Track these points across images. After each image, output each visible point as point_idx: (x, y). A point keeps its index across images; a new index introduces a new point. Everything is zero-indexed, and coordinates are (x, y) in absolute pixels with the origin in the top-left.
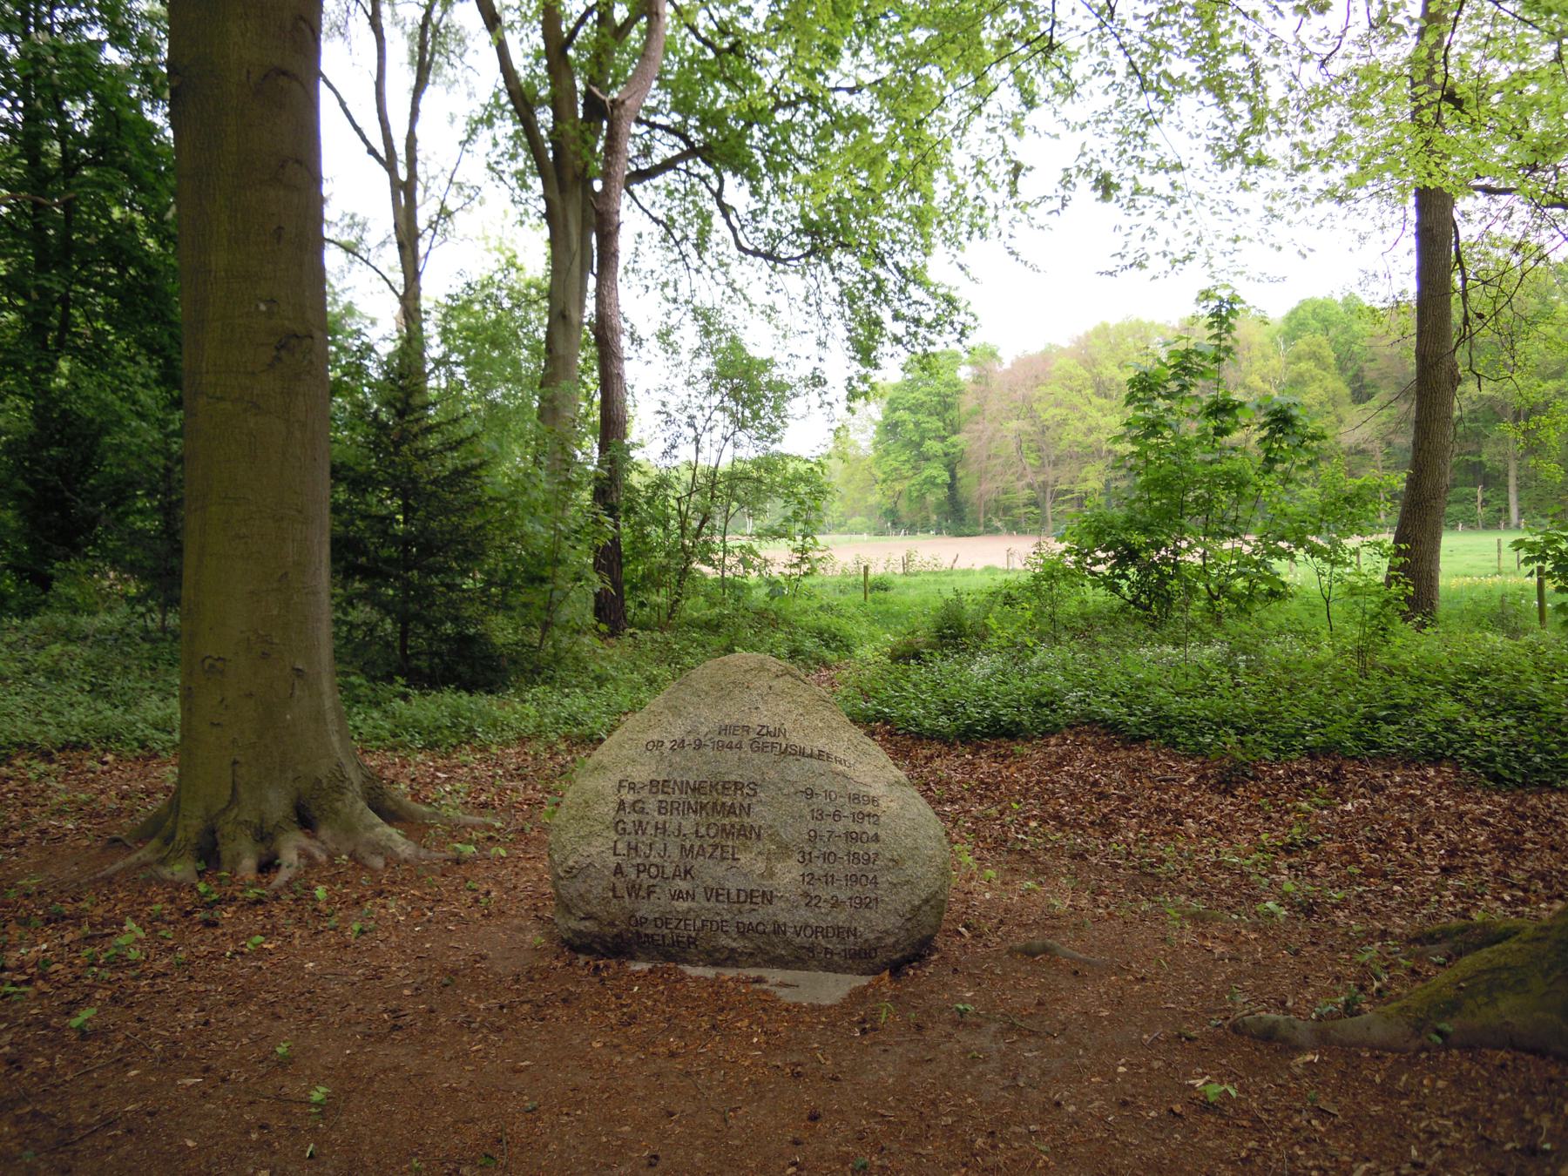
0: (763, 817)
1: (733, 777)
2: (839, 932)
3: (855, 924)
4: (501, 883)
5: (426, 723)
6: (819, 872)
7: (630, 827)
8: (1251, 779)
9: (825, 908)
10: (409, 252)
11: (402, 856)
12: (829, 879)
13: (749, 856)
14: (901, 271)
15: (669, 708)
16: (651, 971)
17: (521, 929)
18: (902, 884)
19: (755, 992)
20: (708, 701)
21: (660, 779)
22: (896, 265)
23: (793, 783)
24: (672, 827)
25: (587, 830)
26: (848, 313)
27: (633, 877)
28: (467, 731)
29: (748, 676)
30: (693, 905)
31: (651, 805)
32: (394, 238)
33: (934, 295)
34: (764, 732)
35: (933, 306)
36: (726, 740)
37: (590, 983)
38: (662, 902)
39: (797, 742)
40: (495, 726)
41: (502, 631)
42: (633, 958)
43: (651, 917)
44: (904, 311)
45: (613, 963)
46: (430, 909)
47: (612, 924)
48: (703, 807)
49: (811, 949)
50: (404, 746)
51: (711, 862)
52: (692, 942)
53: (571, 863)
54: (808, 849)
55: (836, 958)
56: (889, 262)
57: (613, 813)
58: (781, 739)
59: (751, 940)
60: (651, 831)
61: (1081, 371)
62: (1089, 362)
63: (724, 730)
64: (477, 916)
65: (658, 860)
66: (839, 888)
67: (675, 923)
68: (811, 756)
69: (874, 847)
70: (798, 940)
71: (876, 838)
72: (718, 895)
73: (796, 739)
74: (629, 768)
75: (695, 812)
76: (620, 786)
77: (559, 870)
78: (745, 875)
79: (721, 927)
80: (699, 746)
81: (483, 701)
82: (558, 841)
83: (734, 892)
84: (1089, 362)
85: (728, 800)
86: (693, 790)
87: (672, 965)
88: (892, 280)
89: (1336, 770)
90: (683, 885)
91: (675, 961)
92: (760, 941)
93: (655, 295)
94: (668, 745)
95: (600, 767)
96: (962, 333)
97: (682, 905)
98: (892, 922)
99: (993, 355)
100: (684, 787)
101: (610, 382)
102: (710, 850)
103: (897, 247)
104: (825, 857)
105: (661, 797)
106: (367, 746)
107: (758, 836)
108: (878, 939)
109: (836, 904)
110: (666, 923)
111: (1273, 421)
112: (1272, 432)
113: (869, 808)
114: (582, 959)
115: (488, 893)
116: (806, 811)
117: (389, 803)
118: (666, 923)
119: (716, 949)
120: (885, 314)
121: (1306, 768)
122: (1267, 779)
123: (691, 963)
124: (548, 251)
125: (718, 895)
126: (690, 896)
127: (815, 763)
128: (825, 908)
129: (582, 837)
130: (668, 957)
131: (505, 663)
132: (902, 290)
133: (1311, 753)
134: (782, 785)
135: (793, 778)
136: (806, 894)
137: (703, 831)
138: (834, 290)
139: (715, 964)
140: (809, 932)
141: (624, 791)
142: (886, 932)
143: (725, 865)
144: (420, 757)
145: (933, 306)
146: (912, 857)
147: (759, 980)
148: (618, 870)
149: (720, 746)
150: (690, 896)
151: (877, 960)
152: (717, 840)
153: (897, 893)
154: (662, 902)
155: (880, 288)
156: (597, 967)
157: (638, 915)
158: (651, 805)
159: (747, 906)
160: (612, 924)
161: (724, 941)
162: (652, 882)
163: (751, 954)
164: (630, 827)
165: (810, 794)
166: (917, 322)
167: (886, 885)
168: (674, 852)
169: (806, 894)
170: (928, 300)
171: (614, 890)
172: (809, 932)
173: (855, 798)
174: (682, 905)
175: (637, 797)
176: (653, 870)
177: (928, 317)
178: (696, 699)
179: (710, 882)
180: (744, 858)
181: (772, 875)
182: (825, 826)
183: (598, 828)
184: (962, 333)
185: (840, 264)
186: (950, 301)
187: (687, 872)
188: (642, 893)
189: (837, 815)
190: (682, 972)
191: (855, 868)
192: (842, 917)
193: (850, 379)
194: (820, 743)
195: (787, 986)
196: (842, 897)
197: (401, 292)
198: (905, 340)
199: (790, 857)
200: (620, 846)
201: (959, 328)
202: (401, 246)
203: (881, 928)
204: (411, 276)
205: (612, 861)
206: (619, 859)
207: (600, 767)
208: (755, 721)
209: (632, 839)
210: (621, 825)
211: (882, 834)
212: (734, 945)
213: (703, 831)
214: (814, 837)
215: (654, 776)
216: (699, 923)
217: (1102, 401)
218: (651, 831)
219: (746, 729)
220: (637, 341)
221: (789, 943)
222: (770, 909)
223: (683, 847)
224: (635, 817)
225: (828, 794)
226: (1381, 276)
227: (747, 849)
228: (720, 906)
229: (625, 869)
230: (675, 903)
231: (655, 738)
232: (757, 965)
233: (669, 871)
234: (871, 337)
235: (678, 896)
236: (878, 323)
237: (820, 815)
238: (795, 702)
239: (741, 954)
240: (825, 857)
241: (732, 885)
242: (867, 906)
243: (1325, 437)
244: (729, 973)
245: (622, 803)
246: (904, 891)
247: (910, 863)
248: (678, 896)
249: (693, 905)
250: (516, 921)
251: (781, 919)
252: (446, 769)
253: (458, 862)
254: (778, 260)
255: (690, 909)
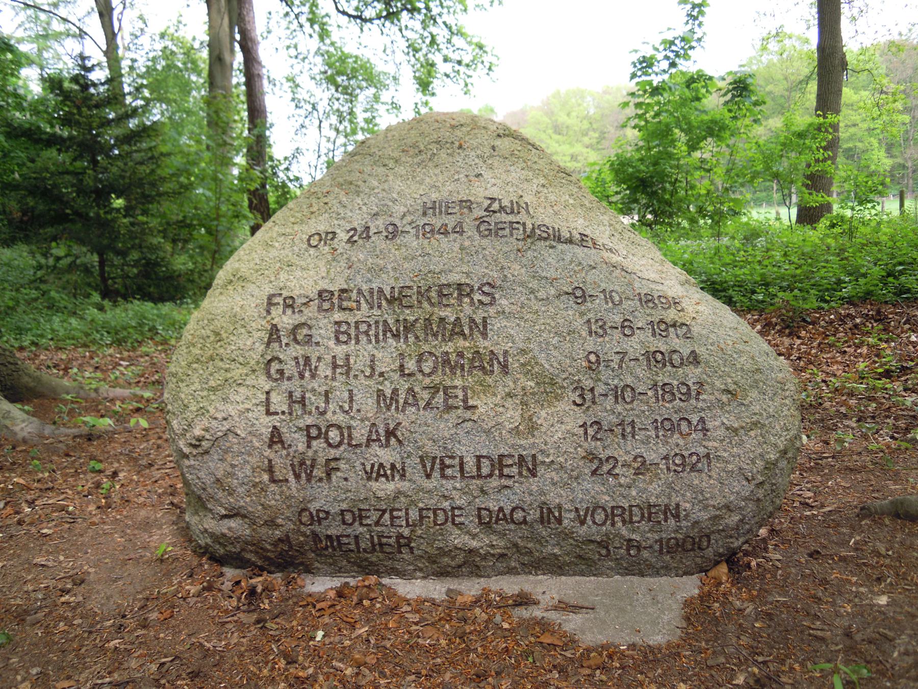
0: (510, 337)
1: (454, 278)
2: (649, 511)
3: (675, 499)
4: (136, 460)
5: (113, 324)
6: (609, 420)
7: (290, 368)
8: (809, 323)
9: (625, 476)
10: (106, 19)
11: (21, 435)
12: (626, 429)
13: (491, 401)
14: (449, 28)
15: (340, 185)
16: (340, 594)
17: (147, 525)
18: (748, 429)
19: (522, 622)
20: (401, 170)
21: (335, 288)
22: (444, 23)
23: (552, 281)
24: (359, 363)
25: (220, 376)
26: (413, 60)
27: (301, 447)
28: (150, 330)
29: (458, 133)
30: (405, 485)
31: (323, 329)
32: (96, 9)
33: (470, 43)
34: (493, 207)
35: (470, 51)
36: (437, 222)
37: (240, 625)
38: (352, 484)
39: (547, 221)
40: (173, 325)
41: (181, 263)
42: (309, 570)
43: (334, 509)
44: (451, 55)
45: (277, 578)
46: (31, 503)
47: (271, 523)
48: (409, 327)
49: (603, 545)
50: (94, 342)
51: (429, 415)
52: (404, 543)
53: (198, 432)
54: (588, 383)
55: (645, 554)
56: (438, 20)
57: (261, 348)
58: (522, 217)
59: (502, 535)
60: (324, 370)
61: (546, 119)
62: (550, 113)
63: (431, 208)
64: (92, 508)
65: (340, 418)
66: (646, 442)
67: (375, 516)
68: (570, 241)
69: (693, 374)
70: (583, 530)
71: (695, 359)
72: (443, 467)
73: (544, 217)
74: (283, 276)
75: (396, 336)
76: (270, 303)
77: (181, 444)
78: (488, 432)
79: (452, 517)
80: (393, 233)
81: (166, 308)
82: (176, 398)
83: (470, 462)
84: (550, 113)
85: (449, 314)
86: (390, 302)
87: (373, 579)
88: (441, 33)
89: (879, 312)
90: (386, 455)
91: (378, 573)
92: (516, 535)
93: (283, 52)
94: (343, 236)
95: (239, 279)
96: (490, 69)
97: (385, 488)
98: (739, 488)
99: (492, 111)
100: (376, 297)
101: (256, 112)
102: (426, 395)
103: (445, 11)
104: (618, 394)
105: (338, 316)
106: (61, 344)
107: (505, 367)
108: (715, 518)
109: (642, 467)
110: (360, 517)
111: (734, 89)
112: (734, 96)
113: (671, 315)
114: (230, 573)
115: (115, 474)
116: (579, 323)
117: (26, 379)
118: (360, 517)
119: (442, 552)
120: (437, 58)
121: (852, 311)
122: (822, 323)
123: (401, 574)
124: (206, 19)
125: (443, 467)
126: (398, 471)
127: (579, 251)
128: (625, 476)
129: (214, 389)
130: (366, 568)
131: (182, 281)
132: (449, 41)
133: (850, 302)
134: (534, 284)
135: (551, 274)
136: (591, 456)
137: (411, 365)
138: (403, 44)
139: (442, 573)
140: (600, 517)
141: (276, 312)
142: (727, 507)
143: (452, 417)
144: (111, 351)
145: (470, 51)
146: (755, 385)
147: (524, 600)
148: (276, 438)
149: (426, 232)
150: (398, 471)
151: (709, 552)
152: (437, 379)
153: (741, 444)
154: (352, 484)
155: (433, 42)
156: (252, 592)
157: (313, 507)
158: (323, 329)
159: (495, 482)
160: (271, 523)
161: (458, 539)
162: (333, 453)
163: (503, 556)
164: (290, 368)
165: (580, 296)
166: (459, 63)
167: (721, 432)
168: (367, 404)
169: (591, 456)
170: (466, 46)
171: (270, 470)
172: (600, 517)
173: (648, 300)
174: (385, 488)
175: (298, 319)
176: (334, 434)
177: (467, 59)
178: (381, 170)
179: (431, 449)
180: (483, 405)
181: (532, 428)
182: (612, 344)
183: (237, 372)
184: (490, 69)
185: (406, 26)
186: (481, 47)
187: (390, 433)
188: (318, 472)
189: (627, 327)
190: (392, 593)
191: (667, 409)
192: (655, 488)
193: (416, 104)
194: (577, 224)
195: (575, 608)
196: (651, 457)
197: (104, 48)
198: (452, 75)
199: (558, 398)
200: (275, 398)
201: (488, 65)
202: (101, 15)
203: (719, 501)
204: (110, 36)
205: (265, 424)
206: (275, 420)
207: (239, 279)
208: (479, 192)
209: (295, 386)
210: (275, 366)
211: (701, 351)
212: (474, 544)
213: (411, 365)
214: (594, 365)
215: (324, 285)
216: (414, 515)
217: (557, 137)
218: (324, 370)
219: (467, 204)
220: (272, 82)
221: (567, 535)
222: (534, 484)
223: (380, 394)
224: (297, 351)
225: (608, 296)
226: (768, 14)
227: (487, 389)
228: (449, 484)
229: (287, 436)
230: (374, 485)
231: (322, 228)
232: (511, 571)
233: (360, 434)
234: (429, 73)
235: (378, 472)
236: (433, 65)
237: (599, 328)
238: (530, 168)
239: (484, 558)
240: (618, 394)
241: (467, 450)
242: (693, 468)
243: (764, 103)
244: (470, 588)
245: (274, 333)
246: (751, 441)
247: (754, 394)
248: (378, 472)
249: (405, 485)
250: (143, 513)
251: (553, 498)
252: (130, 359)
253: (90, 438)
254: (365, 20)
255: (399, 493)
